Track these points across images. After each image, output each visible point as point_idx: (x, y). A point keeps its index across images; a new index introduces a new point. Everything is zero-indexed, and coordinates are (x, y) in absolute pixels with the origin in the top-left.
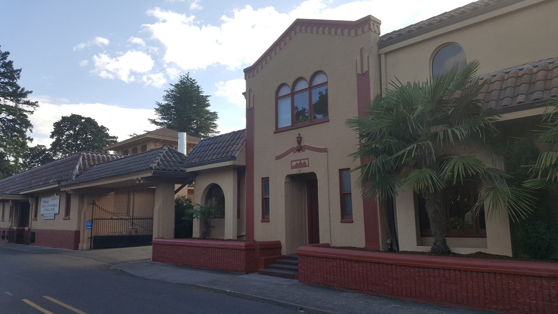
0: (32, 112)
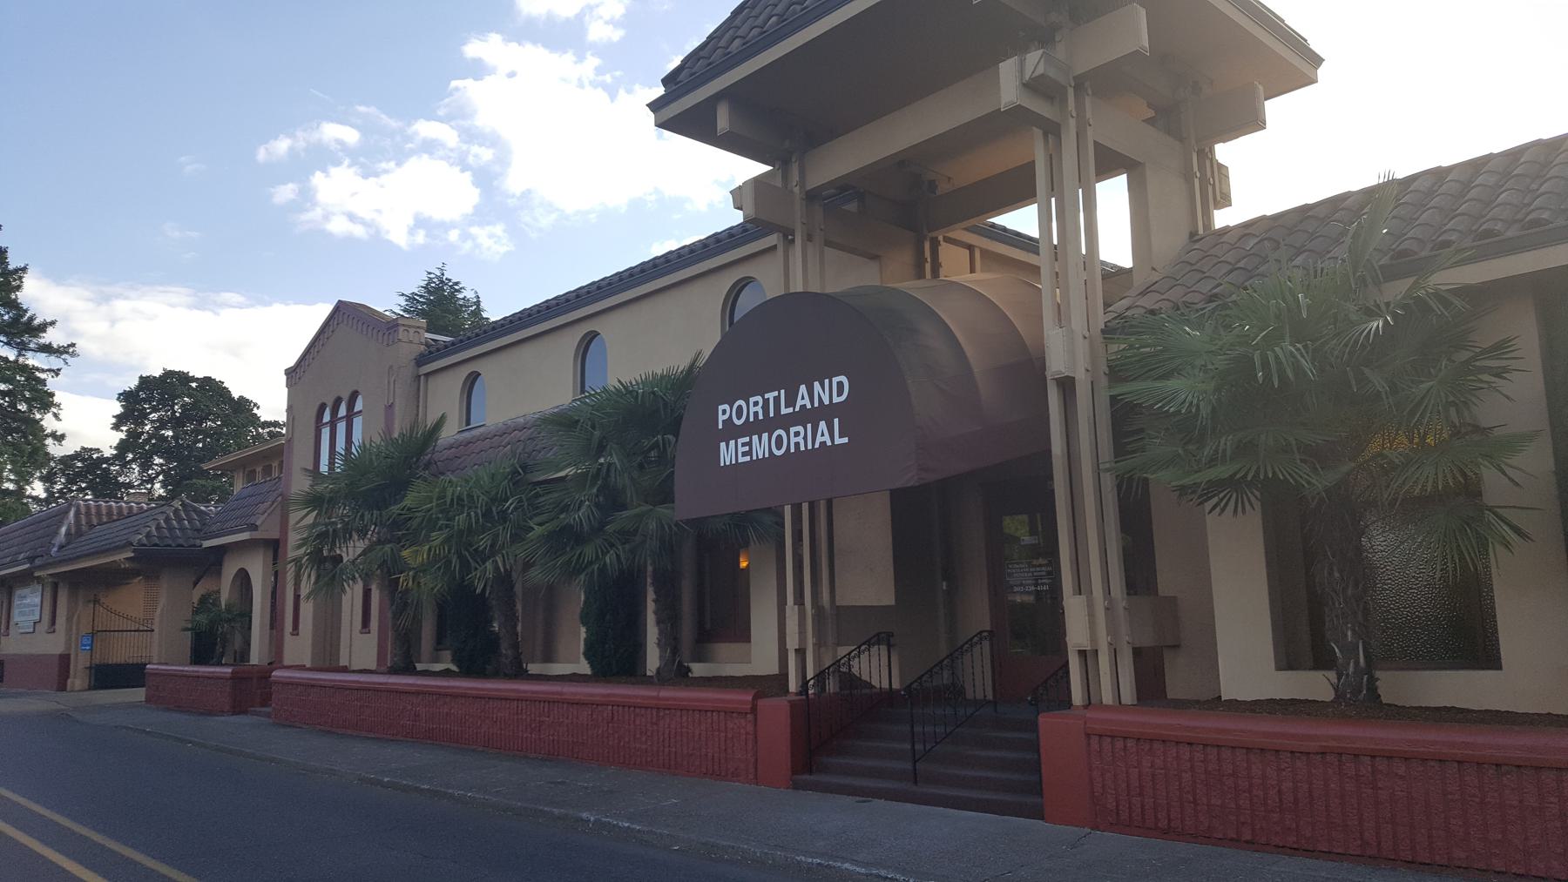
0: (57, 372)
